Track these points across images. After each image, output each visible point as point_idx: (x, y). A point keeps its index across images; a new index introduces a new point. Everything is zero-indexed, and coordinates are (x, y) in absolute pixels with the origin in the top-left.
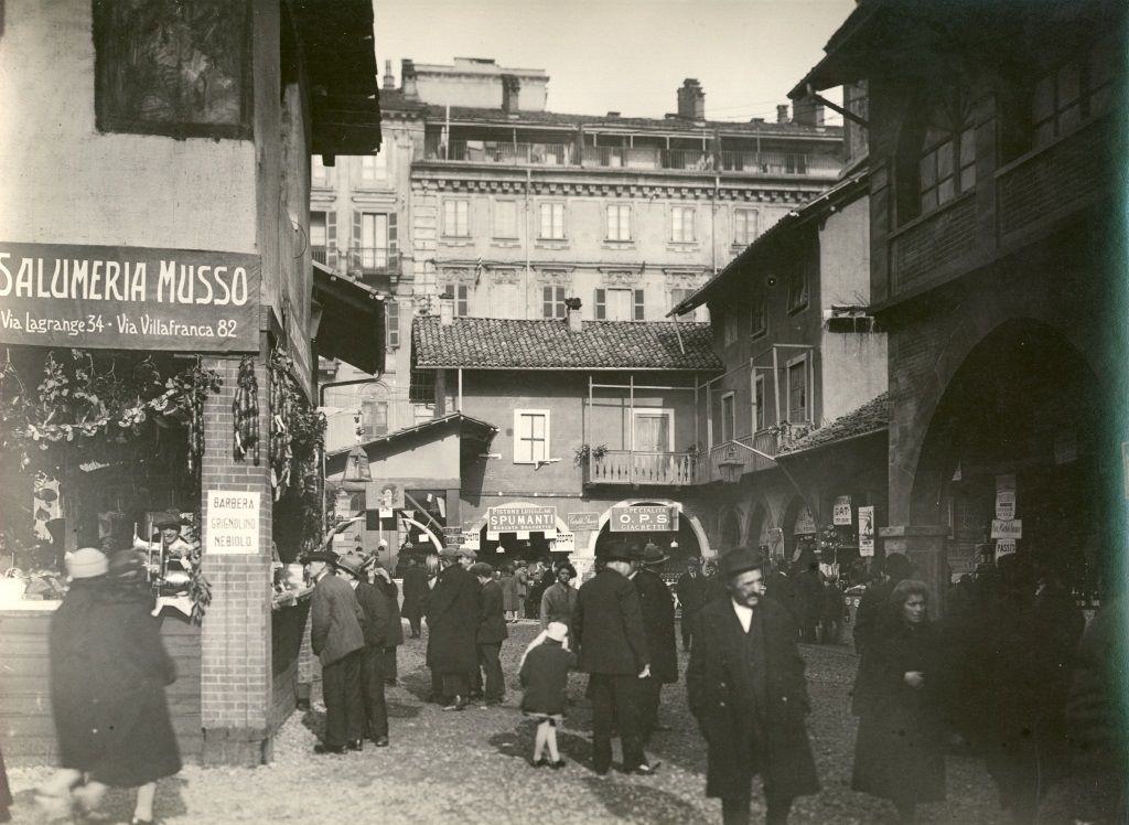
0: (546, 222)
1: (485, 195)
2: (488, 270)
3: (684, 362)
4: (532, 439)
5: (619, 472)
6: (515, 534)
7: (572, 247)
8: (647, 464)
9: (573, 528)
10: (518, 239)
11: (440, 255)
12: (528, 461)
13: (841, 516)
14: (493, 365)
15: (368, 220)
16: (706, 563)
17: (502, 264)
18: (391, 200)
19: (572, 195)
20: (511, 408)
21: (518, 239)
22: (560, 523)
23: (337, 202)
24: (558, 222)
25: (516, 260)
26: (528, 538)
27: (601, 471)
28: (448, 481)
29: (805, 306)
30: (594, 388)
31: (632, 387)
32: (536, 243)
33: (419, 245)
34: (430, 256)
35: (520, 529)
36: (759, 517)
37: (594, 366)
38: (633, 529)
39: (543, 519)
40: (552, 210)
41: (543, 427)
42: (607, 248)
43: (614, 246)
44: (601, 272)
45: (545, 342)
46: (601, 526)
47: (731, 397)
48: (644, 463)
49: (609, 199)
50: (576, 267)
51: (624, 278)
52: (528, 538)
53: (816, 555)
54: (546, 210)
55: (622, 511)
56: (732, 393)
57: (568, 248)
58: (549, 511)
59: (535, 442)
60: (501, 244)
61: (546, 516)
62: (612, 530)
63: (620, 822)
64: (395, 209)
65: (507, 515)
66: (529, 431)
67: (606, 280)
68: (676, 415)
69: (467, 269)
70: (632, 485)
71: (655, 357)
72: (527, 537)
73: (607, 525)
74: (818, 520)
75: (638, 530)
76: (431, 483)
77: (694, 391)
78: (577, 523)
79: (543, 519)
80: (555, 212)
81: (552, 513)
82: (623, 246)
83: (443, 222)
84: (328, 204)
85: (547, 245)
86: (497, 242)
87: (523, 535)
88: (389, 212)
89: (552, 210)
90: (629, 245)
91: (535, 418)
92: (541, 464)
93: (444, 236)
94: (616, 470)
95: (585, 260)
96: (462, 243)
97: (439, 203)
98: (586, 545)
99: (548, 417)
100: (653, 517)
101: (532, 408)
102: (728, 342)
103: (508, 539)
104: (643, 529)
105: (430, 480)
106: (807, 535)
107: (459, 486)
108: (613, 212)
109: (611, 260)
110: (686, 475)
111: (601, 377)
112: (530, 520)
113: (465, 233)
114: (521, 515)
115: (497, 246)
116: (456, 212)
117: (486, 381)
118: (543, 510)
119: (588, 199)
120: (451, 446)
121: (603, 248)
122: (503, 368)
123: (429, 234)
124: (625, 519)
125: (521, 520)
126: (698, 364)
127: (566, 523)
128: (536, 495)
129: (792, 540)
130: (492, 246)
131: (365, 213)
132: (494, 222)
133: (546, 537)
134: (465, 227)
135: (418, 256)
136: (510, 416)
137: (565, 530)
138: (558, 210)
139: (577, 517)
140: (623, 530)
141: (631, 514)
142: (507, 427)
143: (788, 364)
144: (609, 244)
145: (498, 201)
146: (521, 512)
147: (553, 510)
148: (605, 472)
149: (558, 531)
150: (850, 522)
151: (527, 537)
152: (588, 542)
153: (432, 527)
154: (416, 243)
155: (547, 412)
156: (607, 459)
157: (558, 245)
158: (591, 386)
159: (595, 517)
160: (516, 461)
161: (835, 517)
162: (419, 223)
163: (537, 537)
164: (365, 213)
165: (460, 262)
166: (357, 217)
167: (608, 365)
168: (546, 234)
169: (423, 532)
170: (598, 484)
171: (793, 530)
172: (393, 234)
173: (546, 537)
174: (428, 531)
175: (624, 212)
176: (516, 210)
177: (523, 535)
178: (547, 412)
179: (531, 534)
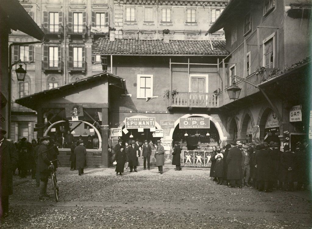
0: (164, 15)
1: (141, 6)
2: (142, 33)
3: (212, 52)
4: (145, 88)
5: (183, 102)
6: (137, 129)
7: (174, 25)
9: (163, 127)
10: (153, 22)
11: (124, 28)
12: (144, 97)
13: (295, 117)
14: (126, 54)
16: (222, 143)
17: (147, 31)
18: (106, 8)
20: (136, 74)
22: (157, 125)
24: (169, 16)
25: (153, 30)
26: (143, 131)
27: (175, 101)
31: (189, 64)
32: (160, 23)
33: (116, 24)
34: (120, 28)
38: (189, 127)
39: (150, 123)
40: (166, 11)
41: (150, 82)
42: (187, 25)
43: (189, 24)
44: (184, 34)
46: (175, 127)
47: (234, 67)
48: (194, 98)
49: (187, 7)
50: (175, 32)
51: (193, 36)
52: (143, 131)
54: (164, 11)
55: (184, 119)
56: (234, 65)
57: (172, 25)
59: (146, 89)
60: (147, 24)
61: (151, 122)
62: (180, 128)
63: (311, 14)
64: (108, 11)
65: (134, 121)
66: (143, 85)
67: (186, 37)
68: (209, 77)
69: (134, 33)
70: (189, 108)
71: (199, 51)
72: (142, 131)
73: (178, 125)
74: (280, 119)
75: (191, 128)
76: (95, 105)
78: (165, 124)
79: (150, 123)
81: (154, 120)
82: (193, 24)
84: (83, 9)
85: (164, 24)
86: (145, 23)
87: (141, 130)
88: (106, 12)
90: (195, 24)
92: (149, 99)
93: (126, 21)
94: (181, 101)
99: (152, 78)
100: (198, 122)
101: (145, 74)
102: (233, 42)
103: (134, 131)
104: (194, 127)
105: (95, 104)
106: (273, 128)
107: (107, 107)
108: (189, 11)
110: (213, 103)
112: (144, 123)
113: (134, 20)
114: (140, 121)
115: (145, 24)
117: (124, 61)
118: (150, 119)
119: (180, 6)
120: (103, 89)
121: (185, 25)
122: (131, 55)
123: (121, 20)
124: (186, 123)
125: (140, 123)
126: (219, 53)
127: (160, 124)
128: (146, 112)
130: (144, 24)
131: (97, 13)
133: (151, 131)
135: (117, 29)
136: (135, 78)
137: (159, 128)
139: (165, 122)
140: (185, 128)
141: (189, 121)
142: (134, 82)
143: (264, 42)
144: (187, 24)
146: (140, 120)
147: (154, 119)
148: (176, 102)
149: (156, 128)
150: (301, 120)
151: (142, 131)
152: (169, 133)
153: (95, 126)
155: (152, 76)
156: (177, 96)
157: (168, 24)
158: (170, 63)
159: (173, 122)
160: (138, 97)
161: (291, 118)
162: (117, 16)
163: (147, 131)
164: (97, 13)
165: (132, 30)
166: (94, 14)
168: (164, 20)
169: (91, 127)
170: (173, 107)
172: (107, 20)
173: (151, 131)
174: (94, 127)
175: (193, 12)
176: (153, 11)
177: (141, 130)
178: (152, 76)
179: (144, 129)
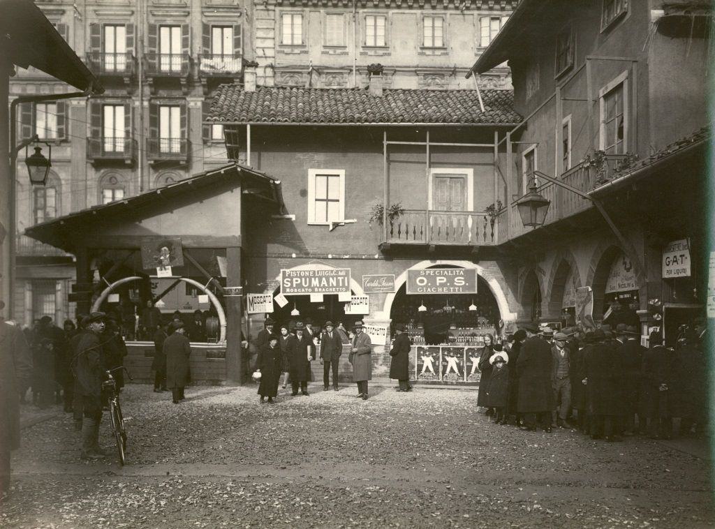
0: (370, 32)
1: (317, 9)
2: (320, 74)
5: (415, 232)
6: (337, 295)
7: (393, 53)
8: (443, 223)
9: (367, 290)
11: (278, 61)
13: (674, 267)
14: (282, 121)
15: (217, 32)
19: (393, 8)
20: (305, 168)
21: (346, 47)
22: (354, 285)
23: (189, 18)
24: (381, 32)
25: (344, 65)
27: (396, 230)
28: (227, 238)
29: (625, 14)
30: (388, 145)
31: (428, 144)
33: (260, 52)
34: (269, 61)
35: (313, 291)
36: (564, 274)
37: (388, 121)
38: (430, 291)
39: (338, 282)
40: (375, 21)
41: (338, 187)
43: (428, 52)
44: (418, 75)
45: (343, 104)
47: (532, 152)
48: (440, 223)
49: (424, 11)
50: (395, 71)
53: (638, 316)
54: (370, 21)
55: (418, 273)
56: (533, 146)
57: (389, 54)
58: (343, 273)
59: (329, 203)
61: (340, 278)
62: (408, 293)
66: (323, 194)
68: (475, 174)
69: (301, 73)
71: (452, 114)
72: (321, 299)
73: (403, 287)
74: (641, 273)
77: (493, 148)
79: (338, 282)
80: (378, 24)
83: (281, 33)
84: (182, 18)
85: (371, 52)
86: (327, 50)
87: (317, 298)
89: (375, 21)
90: (443, 51)
91: (330, 178)
92: (336, 225)
94: (411, 230)
95: (404, 65)
96: (297, 51)
97: (278, 17)
98: (381, 308)
99: (342, 178)
101: (327, 168)
103: (300, 301)
104: (440, 291)
105: (209, 237)
107: (239, 244)
108: (428, 23)
109: (427, 65)
110: (485, 234)
111: (395, 133)
112: (324, 282)
113: (300, 42)
114: (315, 277)
115: (327, 53)
116: (292, 24)
118: (337, 272)
119: (407, 11)
121: (420, 54)
123: (269, 43)
124: (422, 281)
125: (315, 282)
128: (330, 256)
129: (603, 300)
131: (213, 26)
132: (325, 33)
133: (341, 300)
134: (300, 36)
137: (360, 292)
138: (381, 22)
139: (372, 280)
140: (420, 292)
141: (428, 277)
143: (602, 93)
145: (328, 14)
148: (399, 232)
149: (353, 293)
151: (321, 299)
152: (383, 304)
154: (258, 51)
155: (342, 172)
157: (381, 52)
158: (385, 143)
159: (391, 279)
161: (665, 269)
162: (260, 34)
163: (331, 300)
164: (213, 26)
167: (402, 121)
168: (370, 43)
171: (605, 287)
173: (341, 300)
178: (342, 172)
179: (325, 296)
